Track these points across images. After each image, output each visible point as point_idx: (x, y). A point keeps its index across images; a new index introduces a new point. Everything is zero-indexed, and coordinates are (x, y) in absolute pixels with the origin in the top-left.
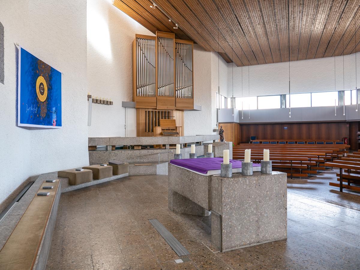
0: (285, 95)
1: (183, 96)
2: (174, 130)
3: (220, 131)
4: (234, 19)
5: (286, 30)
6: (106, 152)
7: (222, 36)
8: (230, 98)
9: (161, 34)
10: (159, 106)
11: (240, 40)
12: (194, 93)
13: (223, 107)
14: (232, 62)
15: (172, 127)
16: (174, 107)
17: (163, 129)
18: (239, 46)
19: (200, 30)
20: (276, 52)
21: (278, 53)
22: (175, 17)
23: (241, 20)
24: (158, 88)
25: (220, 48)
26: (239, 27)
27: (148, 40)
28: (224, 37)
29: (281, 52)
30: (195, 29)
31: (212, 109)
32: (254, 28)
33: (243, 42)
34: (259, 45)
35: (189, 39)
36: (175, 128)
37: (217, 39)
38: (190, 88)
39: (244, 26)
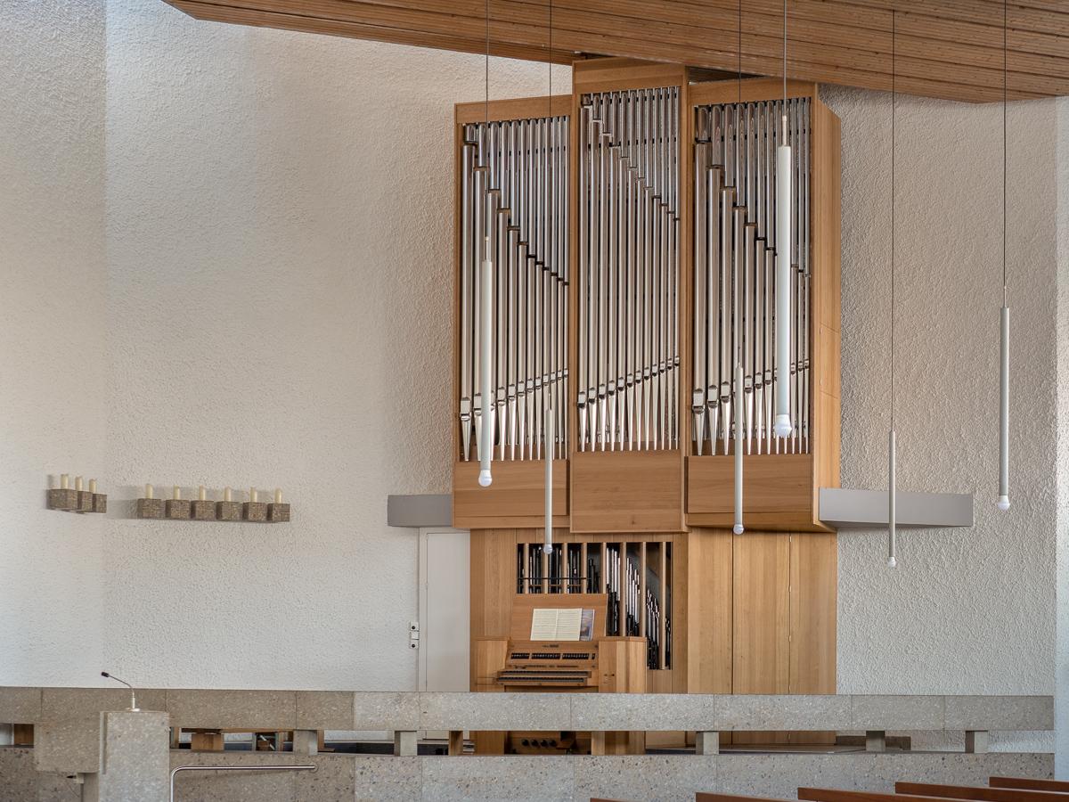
2: (584, 657)
6: (25, 756)
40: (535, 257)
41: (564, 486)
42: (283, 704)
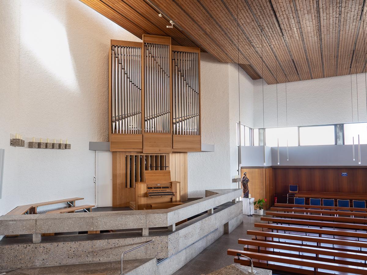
0: (343, 124)
1: (185, 132)
2: (168, 188)
3: (243, 181)
4: (265, 5)
5: (355, 21)
6: (28, 247)
7: (245, 38)
8: (258, 129)
9: (149, 39)
10: (145, 148)
11: (274, 43)
12: (202, 126)
13: (248, 144)
14: (260, 78)
15: (164, 183)
16: (170, 148)
17: (150, 186)
18: (272, 52)
19: (208, 28)
20: (331, 61)
21: (333, 62)
22: (165, 5)
23: (278, 5)
24: (145, 121)
25: (241, 57)
26: (274, 19)
27: (122, 47)
28: (248, 38)
29: (339, 60)
30: (199, 26)
31: (231, 150)
32: (299, 20)
33: (278, 47)
34: (305, 50)
35: (194, 44)
36: (169, 185)
37: (236, 42)
38: (196, 119)
39: (282, 18)
40: (132, 82)
41: (142, 141)
42: (141, 219)
